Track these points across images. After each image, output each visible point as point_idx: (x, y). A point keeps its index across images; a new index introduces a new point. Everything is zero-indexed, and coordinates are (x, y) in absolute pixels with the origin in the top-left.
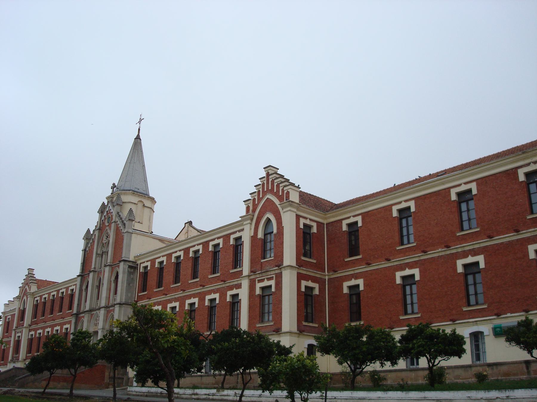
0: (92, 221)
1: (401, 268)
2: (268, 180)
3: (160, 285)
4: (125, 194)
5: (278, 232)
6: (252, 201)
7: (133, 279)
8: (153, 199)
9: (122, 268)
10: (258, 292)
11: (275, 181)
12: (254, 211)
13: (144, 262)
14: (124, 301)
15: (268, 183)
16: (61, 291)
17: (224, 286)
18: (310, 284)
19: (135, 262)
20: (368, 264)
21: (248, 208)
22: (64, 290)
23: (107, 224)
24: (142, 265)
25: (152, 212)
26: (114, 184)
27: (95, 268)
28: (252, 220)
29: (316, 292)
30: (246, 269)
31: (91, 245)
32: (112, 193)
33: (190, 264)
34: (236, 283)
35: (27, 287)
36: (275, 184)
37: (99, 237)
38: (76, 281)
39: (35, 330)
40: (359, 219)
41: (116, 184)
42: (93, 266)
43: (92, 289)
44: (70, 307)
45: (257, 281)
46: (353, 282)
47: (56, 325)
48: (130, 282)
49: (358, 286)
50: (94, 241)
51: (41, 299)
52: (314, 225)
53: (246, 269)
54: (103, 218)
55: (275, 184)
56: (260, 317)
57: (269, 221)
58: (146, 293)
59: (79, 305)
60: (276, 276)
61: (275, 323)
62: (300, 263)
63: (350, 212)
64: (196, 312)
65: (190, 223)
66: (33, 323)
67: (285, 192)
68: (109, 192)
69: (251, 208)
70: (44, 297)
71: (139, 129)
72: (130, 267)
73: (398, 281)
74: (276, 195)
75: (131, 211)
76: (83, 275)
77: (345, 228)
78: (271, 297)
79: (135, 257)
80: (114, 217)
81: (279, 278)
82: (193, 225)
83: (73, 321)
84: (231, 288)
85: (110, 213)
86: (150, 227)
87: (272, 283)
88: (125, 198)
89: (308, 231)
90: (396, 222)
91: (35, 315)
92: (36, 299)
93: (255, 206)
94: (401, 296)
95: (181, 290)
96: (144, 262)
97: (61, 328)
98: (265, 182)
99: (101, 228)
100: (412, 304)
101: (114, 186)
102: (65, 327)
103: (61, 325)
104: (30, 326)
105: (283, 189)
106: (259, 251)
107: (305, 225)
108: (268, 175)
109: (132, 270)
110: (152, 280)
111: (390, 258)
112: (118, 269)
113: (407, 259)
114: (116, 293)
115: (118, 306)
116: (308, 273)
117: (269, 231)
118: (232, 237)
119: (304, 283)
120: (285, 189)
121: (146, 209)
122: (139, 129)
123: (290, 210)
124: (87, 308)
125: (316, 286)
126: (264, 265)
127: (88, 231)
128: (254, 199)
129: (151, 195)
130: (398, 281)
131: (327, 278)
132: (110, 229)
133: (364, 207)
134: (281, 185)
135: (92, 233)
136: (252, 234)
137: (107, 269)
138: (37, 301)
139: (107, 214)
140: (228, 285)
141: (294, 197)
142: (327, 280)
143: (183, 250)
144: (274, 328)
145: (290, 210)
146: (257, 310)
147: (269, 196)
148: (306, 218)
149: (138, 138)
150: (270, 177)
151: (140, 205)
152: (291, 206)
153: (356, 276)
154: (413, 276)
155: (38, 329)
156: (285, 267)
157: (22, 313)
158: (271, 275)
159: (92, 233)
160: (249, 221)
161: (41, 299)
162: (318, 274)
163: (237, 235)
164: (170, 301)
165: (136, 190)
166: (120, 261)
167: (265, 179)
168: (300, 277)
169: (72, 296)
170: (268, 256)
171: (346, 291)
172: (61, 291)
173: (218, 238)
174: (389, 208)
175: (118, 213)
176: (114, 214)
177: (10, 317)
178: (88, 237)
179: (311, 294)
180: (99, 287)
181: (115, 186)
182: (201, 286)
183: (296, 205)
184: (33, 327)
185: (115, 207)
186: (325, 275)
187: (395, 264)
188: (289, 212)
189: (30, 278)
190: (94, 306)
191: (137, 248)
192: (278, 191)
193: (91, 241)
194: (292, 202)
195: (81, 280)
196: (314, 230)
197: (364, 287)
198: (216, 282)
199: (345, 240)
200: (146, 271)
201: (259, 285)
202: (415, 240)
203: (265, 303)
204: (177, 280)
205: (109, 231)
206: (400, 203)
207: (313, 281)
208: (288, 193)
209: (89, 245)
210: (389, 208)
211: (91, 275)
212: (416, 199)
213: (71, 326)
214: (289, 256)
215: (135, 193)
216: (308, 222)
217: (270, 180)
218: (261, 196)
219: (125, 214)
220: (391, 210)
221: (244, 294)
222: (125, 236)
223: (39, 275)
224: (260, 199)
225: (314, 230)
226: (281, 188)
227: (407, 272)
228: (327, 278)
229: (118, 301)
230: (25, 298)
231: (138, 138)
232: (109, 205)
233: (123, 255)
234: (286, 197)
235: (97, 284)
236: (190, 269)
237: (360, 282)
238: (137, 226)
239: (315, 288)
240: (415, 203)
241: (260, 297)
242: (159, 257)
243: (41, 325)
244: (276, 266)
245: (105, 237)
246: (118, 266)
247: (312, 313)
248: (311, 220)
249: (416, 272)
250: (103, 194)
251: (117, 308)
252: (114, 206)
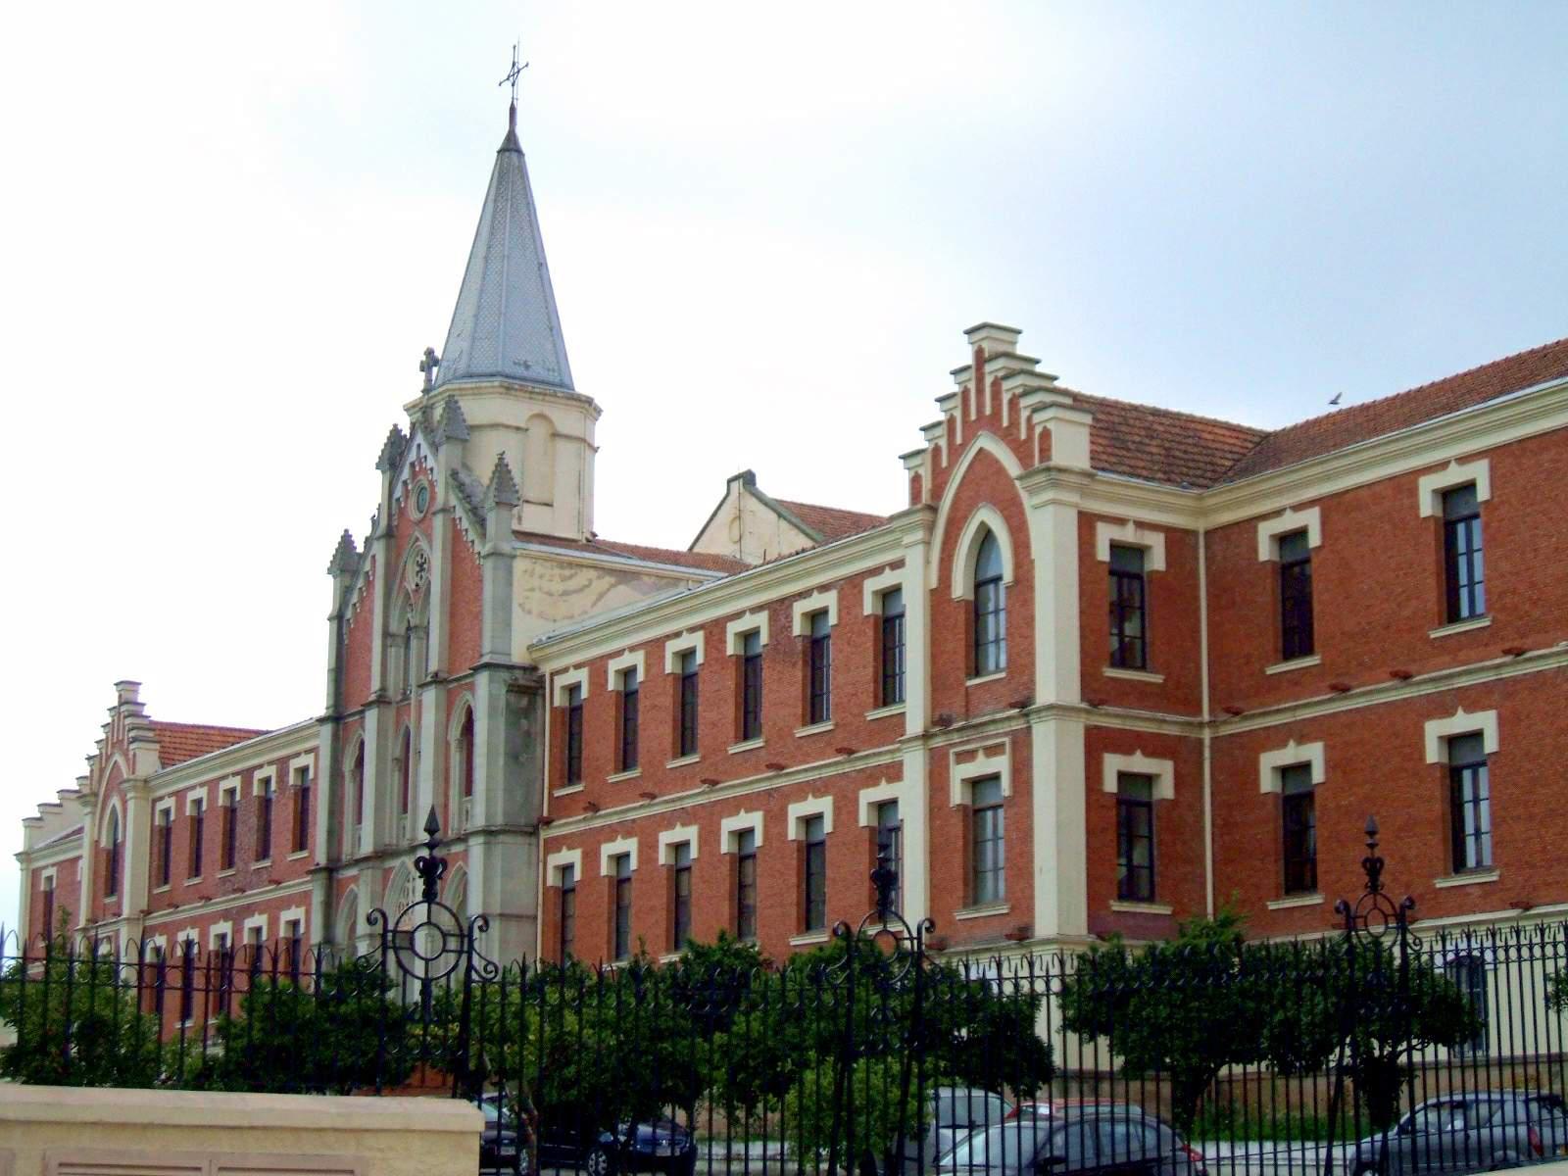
0: (358, 503)
1: (1442, 707)
2: (980, 380)
3: (626, 761)
4: (477, 392)
5: (1017, 581)
6: (928, 457)
7: (528, 734)
8: (589, 401)
9: (484, 694)
10: (957, 795)
11: (1006, 385)
12: (937, 492)
13: (566, 670)
14: (499, 820)
15: (980, 391)
16: (259, 775)
17: (847, 768)
18: (1139, 763)
19: (534, 669)
20: (1342, 690)
21: (916, 481)
22: (271, 771)
23: (414, 515)
24: (562, 681)
25: (588, 452)
26: (430, 353)
27: (383, 689)
28: (931, 528)
29: (1165, 790)
30: (915, 706)
31: (362, 599)
32: (426, 391)
33: (731, 684)
34: (885, 760)
35: (118, 758)
36: (1006, 398)
37: (392, 572)
38: (316, 735)
39: (169, 929)
40: (1311, 519)
41: (438, 354)
42: (376, 685)
43: (380, 774)
44: (301, 841)
45: (952, 758)
46: (1290, 754)
47: (249, 910)
48: (518, 753)
49: (1305, 767)
50: (369, 584)
51: (180, 805)
52: (1156, 542)
53: (915, 706)
54: (398, 492)
55: (1006, 398)
56: (966, 884)
57: (986, 537)
58: (579, 788)
59: (334, 834)
60: (1014, 743)
61: (1012, 909)
62: (1095, 692)
63: (1279, 492)
64: (759, 861)
65: (748, 479)
66: (154, 905)
67: (1038, 430)
68: (413, 386)
69: (926, 484)
70: (192, 796)
71: (513, 110)
72: (515, 689)
73: (1433, 753)
74: (1008, 436)
75: (502, 469)
76: (339, 717)
77: (1265, 552)
78: (1001, 812)
79: (530, 648)
80: (440, 490)
81: (1021, 750)
82: (761, 485)
83: (318, 898)
84: (871, 778)
85: (424, 471)
86: (583, 515)
87: (1001, 764)
88: (475, 410)
89: (1133, 568)
90: (1430, 540)
91: (162, 871)
92: (161, 806)
93: (940, 477)
94: (1438, 807)
95: (704, 782)
96: (566, 670)
97: (273, 922)
98: (972, 386)
99: (392, 529)
100: (1478, 833)
101: (430, 362)
102: (287, 915)
103: (273, 908)
104: (147, 913)
105: (1029, 419)
106: (957, 645)
107: (1116, 547)
108: (981, 359)
109: (524, 702)
110: (600, 739)
111: (1413, 668)
112: (469, 696)
113: (1460, 674)
114: (468, 790)
115: (481, 839)
116: (1129, 725)
117: (991, 573)
118: (871, 585)
119: (1113, 764)
120: (1037, 418)
121: (562, 445)
122: (513, 110)
123: (1054, 502)
124: (367, 848)
125: (1164, 770)
126: (974, 699)
127: (346, 540)
128: (937, 451)
129: (581, 387)
130: (1433, 753)
131: (1207, 735)
132: (429, 537)
133: (1328, 477)
134: (1024, 402)
135: (360, 549)
136: (934, 583)
137: (430, 696)
138: (166, 812)
139: (414, 474)
140: (860, 765)
141: (1072, 446)
142: (1207, 742)
143: (701, 627)
144: (1011, 925)
145: (1054, 502)
146: (957, 859)
147: (986, 442)
148: (1121, 521)
149: (511, 147)
150: (988, 368)
151: (539, 431)
152: (1055, 484)
153: (1302, 733)
154: (1477, 736)
155: (181, 925)
156: (1039, 711)
157: (111, 863)
158: (997, 736)
159: (360, 549)
160: (919, 535)
161: (180, 805)
162: (1171, 725)
163: (887, 579)
164: (667, 821)
165: (520, 371)
166: (476, 669)
167: (972, 374)
168: (1097, 743)
169: (303, 794)
170: (992, 666)
171: (1268, 783)
172: (259, 775)
173: (824, 588)
174: (1405, 485)
175: (454, 474)
176: (440, 478)
177: (52, 871)
178: (346, 562)
179: (1144, 798)
180: (404, 765)
181: (436, 362)
182: (770, 767)
183: (1073, 479)
184: (159, 918)
185: (443, 449)
186: (1201, 725)
187: (1429, 689)
188: (1051, 508)
189: (128, 719)
190: (390, 839)
191: (537, 616)
192: (1014, 423)
193: (360, 583)
194: (1060, 470)
195: (336, 737)
196: (1157, 561)
197: (1327, 772)
198: (822, 755)
199: (1266, 598)
200: (575, 704)
201: (960, 772)
202: (1489, 608)
203: (976, 834)
204: (685, 741)
205: (423, 544)
206: (1443, 465)
207: (1150, 753)
208: (1046, 435)
209: (355, 598)
210: (1405, 485)
211: (372, 717)
212: (1494, 455)
213: (308, 913)
214: (1055, 665)
215: (515, 383)
216: (1128, 535)
217: (988, 380)
218: (959, 440)
219: (483, 471)
220: (1413, 492)
221: (911, 797)
222: (488, 566)
223: (160, 708)
224: (956, 452)
225: (1157, 561)
226: (1024, 414)
227: (1461, 722)
228: (1207, 735)
229: (479, 821)
230: (115, 801)
231: (511, 147)
232: (420, 438)
233: (487, 646)
234: (1041, 451)
235: (398, 752)
236: (731, 701)
237: (1314, 753)
238: (534, 520)
239: (1158, 776)
240: (1492, 469)
241: (965, 816)
242: (619, 653)
243: (191, 910)
244: (1013, 706)
245: (412, 569)
246: (471, 688)
247: (1151, 867)
248: (1141, 525)
249: (1486, 721)
250: (392, 398)
251: (476, 846)
252: (435, 447)
